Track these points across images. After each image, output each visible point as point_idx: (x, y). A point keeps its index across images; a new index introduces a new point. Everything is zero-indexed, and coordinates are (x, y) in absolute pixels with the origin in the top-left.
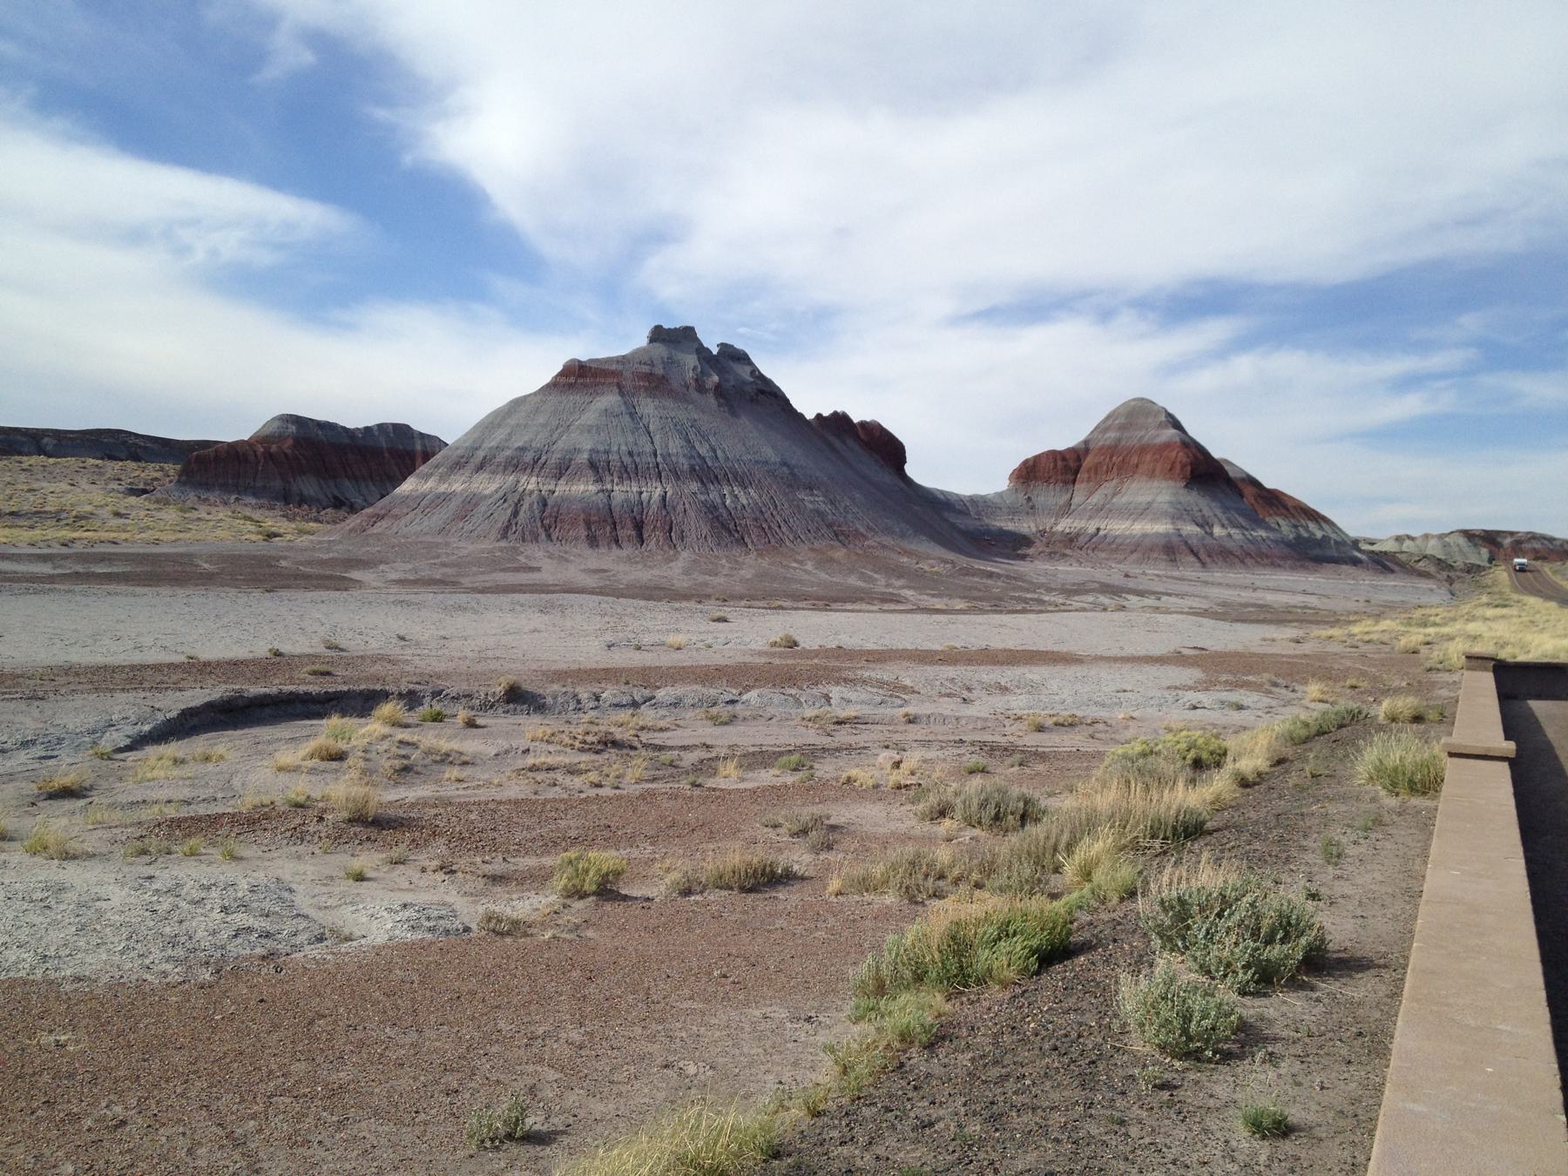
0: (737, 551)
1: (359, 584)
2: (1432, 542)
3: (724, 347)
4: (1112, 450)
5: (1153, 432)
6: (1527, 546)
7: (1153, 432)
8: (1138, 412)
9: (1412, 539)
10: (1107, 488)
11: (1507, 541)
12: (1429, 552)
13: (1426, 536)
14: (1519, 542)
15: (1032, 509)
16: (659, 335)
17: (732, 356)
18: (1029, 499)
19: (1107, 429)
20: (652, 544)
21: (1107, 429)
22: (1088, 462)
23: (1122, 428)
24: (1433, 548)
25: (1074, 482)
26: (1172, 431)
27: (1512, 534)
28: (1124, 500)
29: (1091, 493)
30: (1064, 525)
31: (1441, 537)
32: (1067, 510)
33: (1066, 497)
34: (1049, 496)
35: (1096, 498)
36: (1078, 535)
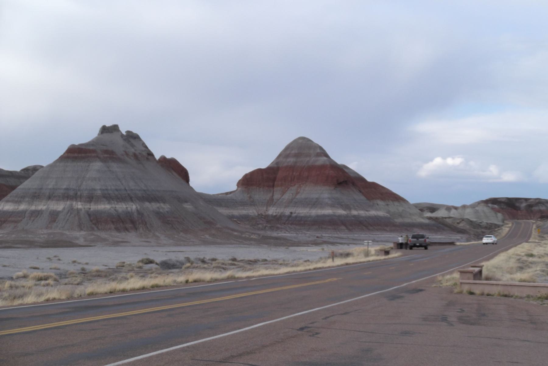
0: (127, 233)
1: (230, 260)
2: (468, 210)
3: (128, 132)
4: (291, 168)
5: (313, 159)
6: (536, 208)
7: (313, 159)
8: (302, 148)
9: (456, 208)
10: (293, 189)
11: (524, 205)
12: (466, 217)
13: (464, 207)
14: (530, 206)
15: (252, 203)
16: (105, 130)
17: (132, 137)
18: (250, 197)
19: (287, 156)
20: (141, 229)
21: (287, 156)
22: (280, 175)
23: (297, 156)
24: (469, 215)
25: (273, 186)
26: (325, 158)
27: (526, 200)
28: (303, 196)
29: (283, 193)
30: (272, 211)
31: (473, 206)
32: (271, 202)
33: (271, 194)
34: (260, 195)
35: (287, 196)
36: (280, 216)
